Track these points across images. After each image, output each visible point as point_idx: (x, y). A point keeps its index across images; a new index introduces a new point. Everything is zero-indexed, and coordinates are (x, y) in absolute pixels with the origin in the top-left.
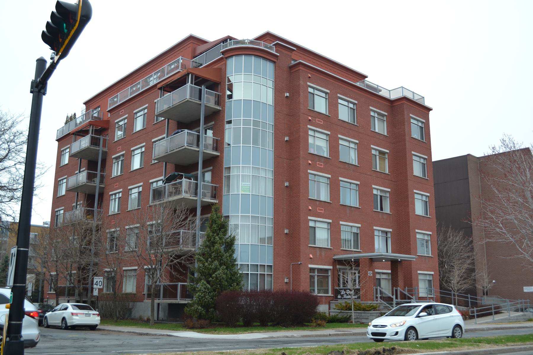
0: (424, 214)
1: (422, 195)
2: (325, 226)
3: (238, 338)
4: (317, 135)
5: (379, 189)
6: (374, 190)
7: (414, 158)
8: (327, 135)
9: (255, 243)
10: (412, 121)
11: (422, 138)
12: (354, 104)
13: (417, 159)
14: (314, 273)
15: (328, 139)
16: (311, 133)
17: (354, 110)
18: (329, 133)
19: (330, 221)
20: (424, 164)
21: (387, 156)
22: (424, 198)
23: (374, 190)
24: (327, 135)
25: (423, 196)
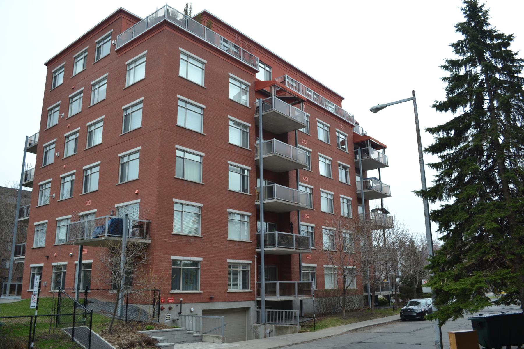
0: (330, 211)
1: (327, 194)
2: (196, 211)
3: (188, 344)
4: (189, 106)
5: (330, 194)
6: (321, 193)
7: (320, 159)
8: (202, 108)
9: (198, 234)
10: (318, 124)
11: (328, 142)
12: (328, 127)
13: (323, 160)
14: (230, 268)
15: (203, 114)
16: (180, 103)
17: (328, 131)
18: (204, 107)
19: (202, 205)
20: (330, 165)
21: (348, 170)
22: (329, 197)
23: (321, 193)
24: (202, 108)
25: (344, 199)
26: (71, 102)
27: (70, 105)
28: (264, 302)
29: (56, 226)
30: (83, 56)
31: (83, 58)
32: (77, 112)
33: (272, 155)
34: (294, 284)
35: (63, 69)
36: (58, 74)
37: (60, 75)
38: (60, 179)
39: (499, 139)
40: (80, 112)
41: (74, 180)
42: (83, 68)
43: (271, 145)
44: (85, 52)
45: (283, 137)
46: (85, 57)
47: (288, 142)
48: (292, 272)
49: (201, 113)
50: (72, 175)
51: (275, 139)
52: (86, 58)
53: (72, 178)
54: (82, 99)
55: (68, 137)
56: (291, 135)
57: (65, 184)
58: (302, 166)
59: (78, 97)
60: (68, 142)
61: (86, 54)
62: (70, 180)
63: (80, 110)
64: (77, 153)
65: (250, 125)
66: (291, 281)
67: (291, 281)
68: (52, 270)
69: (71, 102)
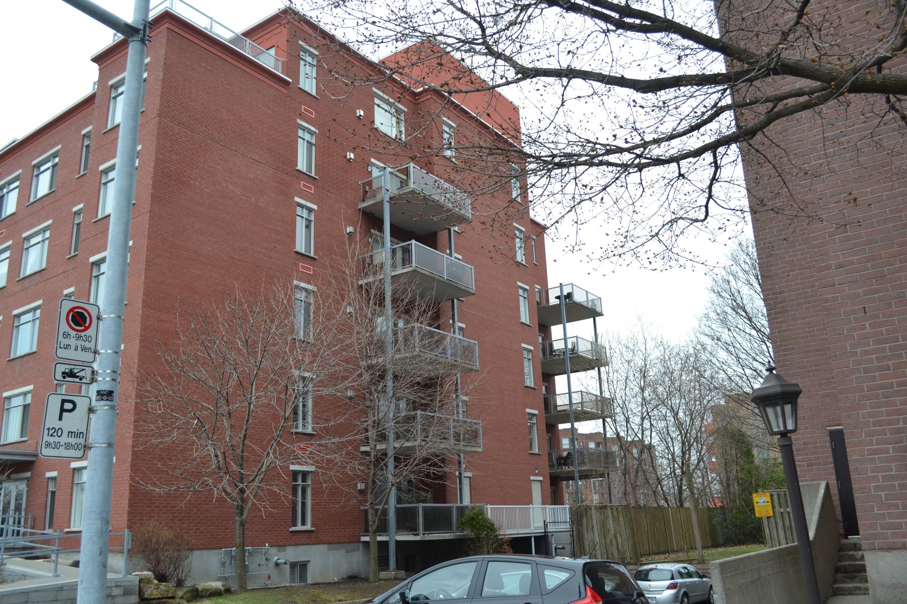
26: (35, 173)
27: (34, 179)
28: (394, 542)
29: (13, 325)
30: (49, 164)
31: (51, 168)
32: (37, 269)
33: (410, 269)
34: (451, 508)
35: (17, 183)
36: (8, 193)
37: (11, 194)
38: (22, 240)
39: (591, 586)
40: (44, 270)
41: (29, 405)
42: (51, 188)
43: (407, 251)
44: (55, 155)
45: (430, 239)
46: (54, 166)
47: (438, 248)
48: (447, 492)
49: (313, 62)
50: (35, 309)
51: (413, 242)
52: (56, 168)
53: (34, 315)
54: (47, 242)
55: (28, 239)
56: (443, 236)
57: (11, 409)
58: (467, 293)
59: (39, 238)
60: (18, 326)
61: (57, 160)
62: (31, 319)
63: (44, 266)
64: (54, 189)
65: (406, 110)
66: (445, 503)
67: (445, 503)
68: (4, 405)
69: (35, 173)
